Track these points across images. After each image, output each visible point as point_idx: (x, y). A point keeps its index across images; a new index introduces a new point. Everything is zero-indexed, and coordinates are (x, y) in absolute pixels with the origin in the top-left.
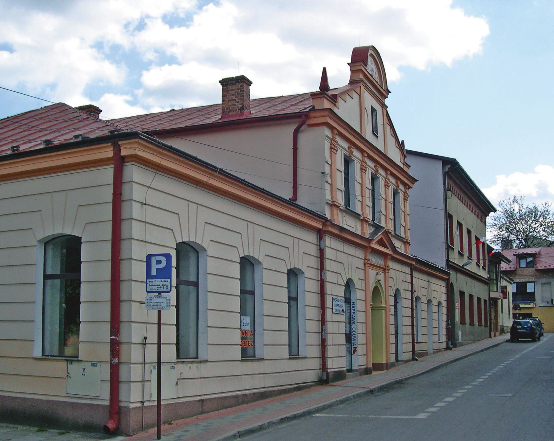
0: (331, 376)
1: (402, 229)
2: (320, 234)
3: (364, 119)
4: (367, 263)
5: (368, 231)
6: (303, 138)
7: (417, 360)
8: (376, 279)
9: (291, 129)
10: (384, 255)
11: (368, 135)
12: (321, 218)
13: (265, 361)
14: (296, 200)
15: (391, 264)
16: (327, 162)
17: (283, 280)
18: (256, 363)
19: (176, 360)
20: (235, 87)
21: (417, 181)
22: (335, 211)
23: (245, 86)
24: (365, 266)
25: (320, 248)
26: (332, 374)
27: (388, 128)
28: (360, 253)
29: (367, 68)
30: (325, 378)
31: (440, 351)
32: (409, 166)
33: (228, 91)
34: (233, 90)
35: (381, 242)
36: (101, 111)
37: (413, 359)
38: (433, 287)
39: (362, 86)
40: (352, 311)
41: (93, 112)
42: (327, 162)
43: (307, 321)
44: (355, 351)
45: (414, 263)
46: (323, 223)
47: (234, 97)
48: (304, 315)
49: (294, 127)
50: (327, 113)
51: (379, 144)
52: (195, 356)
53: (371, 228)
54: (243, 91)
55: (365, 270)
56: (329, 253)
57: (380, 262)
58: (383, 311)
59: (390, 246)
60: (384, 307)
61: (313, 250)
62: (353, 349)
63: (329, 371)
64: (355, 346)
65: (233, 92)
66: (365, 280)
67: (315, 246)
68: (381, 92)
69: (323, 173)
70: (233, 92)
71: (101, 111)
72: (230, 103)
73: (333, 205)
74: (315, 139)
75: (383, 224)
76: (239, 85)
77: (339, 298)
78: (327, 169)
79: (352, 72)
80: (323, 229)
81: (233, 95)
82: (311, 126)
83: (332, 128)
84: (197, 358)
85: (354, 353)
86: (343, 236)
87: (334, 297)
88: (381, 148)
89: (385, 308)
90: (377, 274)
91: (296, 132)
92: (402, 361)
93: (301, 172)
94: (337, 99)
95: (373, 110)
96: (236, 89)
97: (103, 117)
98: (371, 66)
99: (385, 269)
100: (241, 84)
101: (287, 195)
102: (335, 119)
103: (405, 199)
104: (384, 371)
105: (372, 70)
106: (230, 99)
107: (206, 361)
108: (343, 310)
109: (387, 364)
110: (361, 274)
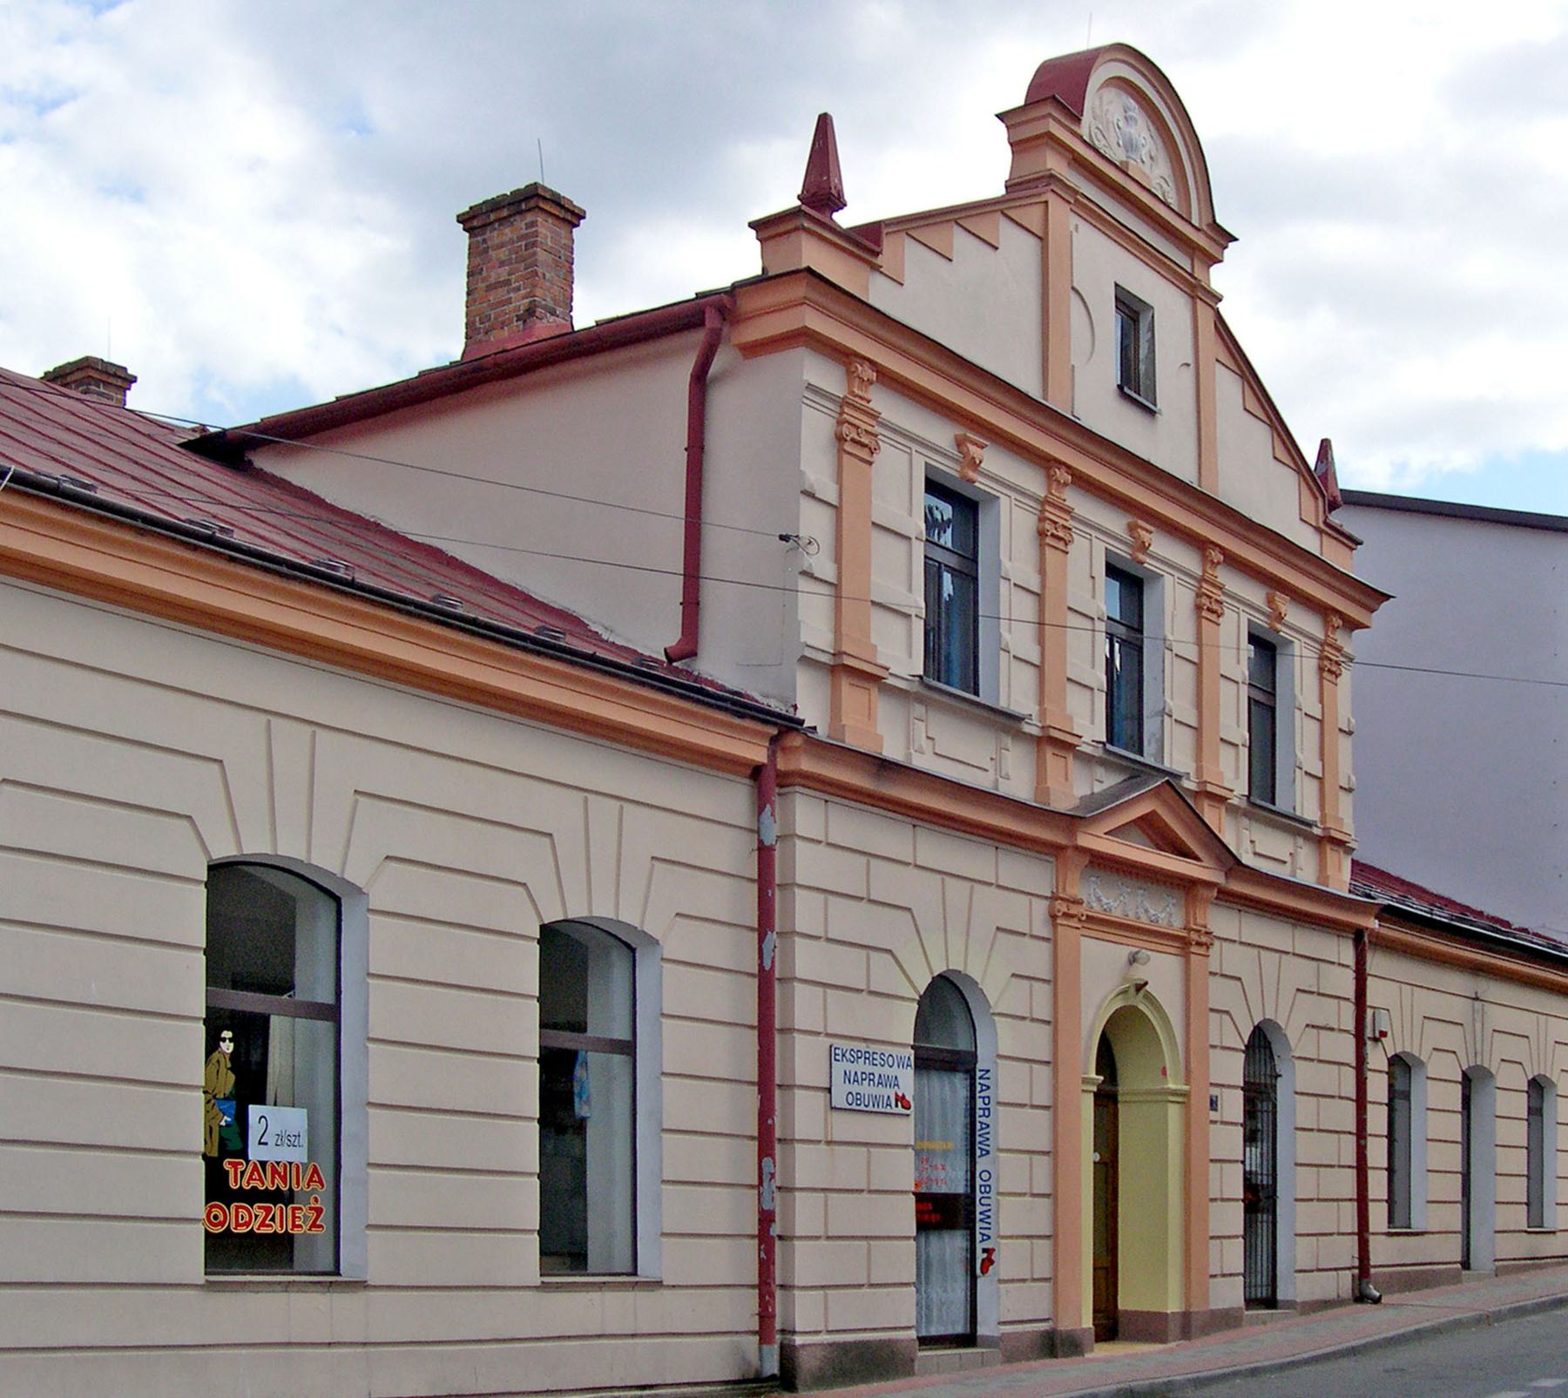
0: (807, 1363)
1: (1311, 787)
2: (764, 782)
3: (1066, 335)
4: (1061, 912)
5: (1074, 786)
6: (724, 403)
7: (1377, 1301)
8: (1125, 979)
9: (679, 373)
10: (1187, 886)
11: (1095, 402)
12: (786, 726)
13: (666, 1292)
14: (693, 654)
15: (1221, 921)
16: (810, 495)
17: (524, 968)
18: (642, 1297)
19: (538, 1280)
20: (508, 233)
21: (1388, 597)
22: (851, 693)
23: (546, 229)
24: (1055, 926)
25: (761, 842)
26: (820, 1353)
27: (1227, 386)
28: (1033, 875)
29: (1084, 131)
30: (772, 1367)
31: (1541, 1267)
32: (1352, 542)
33: (486, 251)
34: (502, 245)
35: (1151, 829)
36: (134, 379)
37: (1361, 1297)
38: (1499, 1017)
39: (1051, 198)
40: (979, 1103)
41: (98, 382)
42: (810, 495)
43: (666, 1136)
44: (988, 1262)
45: (1374, 924)
46: (774, 740)
47: (503, 273)
48: (657, 1112)
49: (687, 366)
50: (799, 290)
51: (1164, 443)
52: (330, 1268)
53: (1100, 772)
54: (534, 244)
55: (1053, 941)
56: (807, 864)
57: (1166, 913)
58: (1174, 1112)
59: (1205, 846)
60: (1175, 1093)
61: (734, 853)
62: (980, 1256)
63: (799, 1340)
64: (986, 1245)
65: (503, 254)
66: (1059, 979)
67: (745, 836)
68: (1189, 240)
69: (784, 538)
70: (503, 254)
71: (134, 379)
72: (493, 297)
73: (841, 669)
74: (781, 410)
75: (1177, 756)
76: (520, 224)
77: (873, 1048)
78: (814, 523)
79: (1018, 146)
80: (775, 758)
81: (502, 264)
82: (753, 349)
83: (843, 356)
84: (635, 1273)
85: (984, 1270)
86: (885, 787)
87: (837, 1042)
88: (1178, 462)
89: (1186, 1094)
90: (1133, 960)
91: (700, 381)
92: (1290, 1304)
93: (715, 541)
94: (878, 242)
95: (1131, 310)
96: (512, 242)
97: (136, 399)
98: (1109, 120)
99: (1187, 944)
100: (529, 218)
101: (653, 636)
102: (864, 323)
103: (1328, 669)
104: (1172, 1345)
105: (1130, 146)
106: (492, 280)
107: (659, 1284)
108: (901, 1100)
109: (1186, 1316)
110: (1037, 959)
